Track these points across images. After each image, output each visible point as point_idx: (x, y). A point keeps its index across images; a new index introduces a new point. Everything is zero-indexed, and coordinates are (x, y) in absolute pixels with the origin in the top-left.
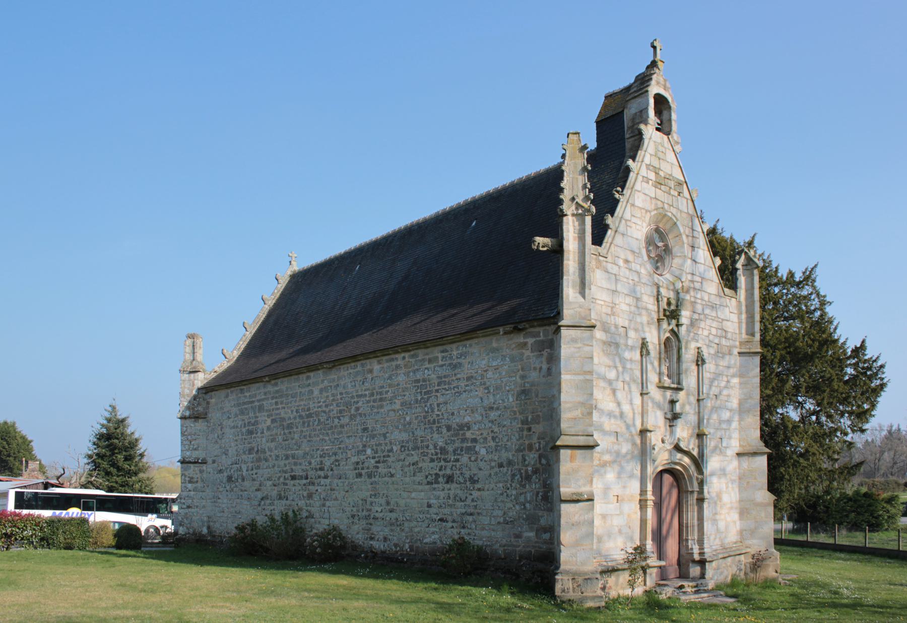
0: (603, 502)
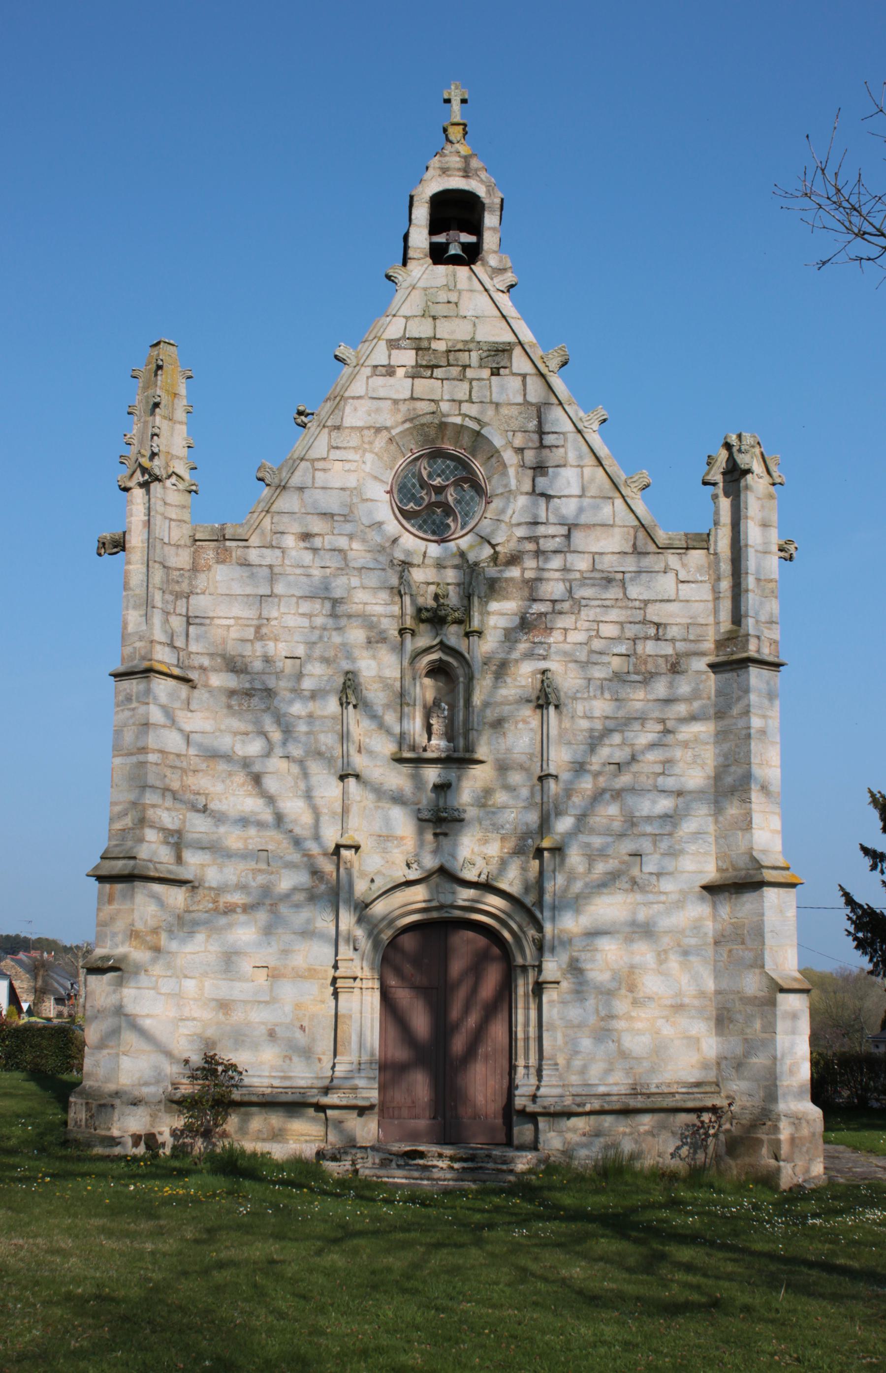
0: (224, 976)
